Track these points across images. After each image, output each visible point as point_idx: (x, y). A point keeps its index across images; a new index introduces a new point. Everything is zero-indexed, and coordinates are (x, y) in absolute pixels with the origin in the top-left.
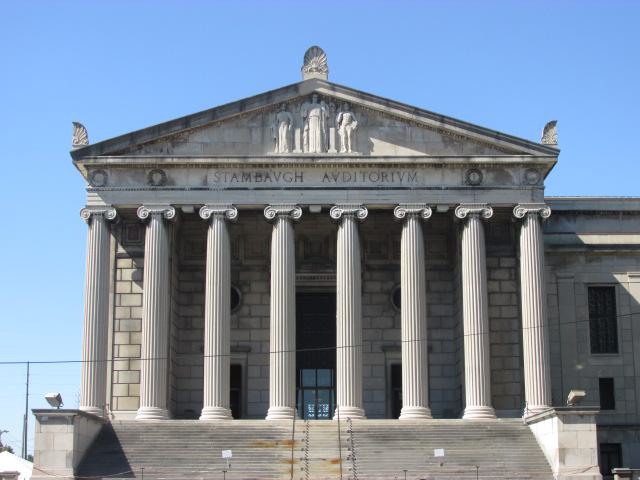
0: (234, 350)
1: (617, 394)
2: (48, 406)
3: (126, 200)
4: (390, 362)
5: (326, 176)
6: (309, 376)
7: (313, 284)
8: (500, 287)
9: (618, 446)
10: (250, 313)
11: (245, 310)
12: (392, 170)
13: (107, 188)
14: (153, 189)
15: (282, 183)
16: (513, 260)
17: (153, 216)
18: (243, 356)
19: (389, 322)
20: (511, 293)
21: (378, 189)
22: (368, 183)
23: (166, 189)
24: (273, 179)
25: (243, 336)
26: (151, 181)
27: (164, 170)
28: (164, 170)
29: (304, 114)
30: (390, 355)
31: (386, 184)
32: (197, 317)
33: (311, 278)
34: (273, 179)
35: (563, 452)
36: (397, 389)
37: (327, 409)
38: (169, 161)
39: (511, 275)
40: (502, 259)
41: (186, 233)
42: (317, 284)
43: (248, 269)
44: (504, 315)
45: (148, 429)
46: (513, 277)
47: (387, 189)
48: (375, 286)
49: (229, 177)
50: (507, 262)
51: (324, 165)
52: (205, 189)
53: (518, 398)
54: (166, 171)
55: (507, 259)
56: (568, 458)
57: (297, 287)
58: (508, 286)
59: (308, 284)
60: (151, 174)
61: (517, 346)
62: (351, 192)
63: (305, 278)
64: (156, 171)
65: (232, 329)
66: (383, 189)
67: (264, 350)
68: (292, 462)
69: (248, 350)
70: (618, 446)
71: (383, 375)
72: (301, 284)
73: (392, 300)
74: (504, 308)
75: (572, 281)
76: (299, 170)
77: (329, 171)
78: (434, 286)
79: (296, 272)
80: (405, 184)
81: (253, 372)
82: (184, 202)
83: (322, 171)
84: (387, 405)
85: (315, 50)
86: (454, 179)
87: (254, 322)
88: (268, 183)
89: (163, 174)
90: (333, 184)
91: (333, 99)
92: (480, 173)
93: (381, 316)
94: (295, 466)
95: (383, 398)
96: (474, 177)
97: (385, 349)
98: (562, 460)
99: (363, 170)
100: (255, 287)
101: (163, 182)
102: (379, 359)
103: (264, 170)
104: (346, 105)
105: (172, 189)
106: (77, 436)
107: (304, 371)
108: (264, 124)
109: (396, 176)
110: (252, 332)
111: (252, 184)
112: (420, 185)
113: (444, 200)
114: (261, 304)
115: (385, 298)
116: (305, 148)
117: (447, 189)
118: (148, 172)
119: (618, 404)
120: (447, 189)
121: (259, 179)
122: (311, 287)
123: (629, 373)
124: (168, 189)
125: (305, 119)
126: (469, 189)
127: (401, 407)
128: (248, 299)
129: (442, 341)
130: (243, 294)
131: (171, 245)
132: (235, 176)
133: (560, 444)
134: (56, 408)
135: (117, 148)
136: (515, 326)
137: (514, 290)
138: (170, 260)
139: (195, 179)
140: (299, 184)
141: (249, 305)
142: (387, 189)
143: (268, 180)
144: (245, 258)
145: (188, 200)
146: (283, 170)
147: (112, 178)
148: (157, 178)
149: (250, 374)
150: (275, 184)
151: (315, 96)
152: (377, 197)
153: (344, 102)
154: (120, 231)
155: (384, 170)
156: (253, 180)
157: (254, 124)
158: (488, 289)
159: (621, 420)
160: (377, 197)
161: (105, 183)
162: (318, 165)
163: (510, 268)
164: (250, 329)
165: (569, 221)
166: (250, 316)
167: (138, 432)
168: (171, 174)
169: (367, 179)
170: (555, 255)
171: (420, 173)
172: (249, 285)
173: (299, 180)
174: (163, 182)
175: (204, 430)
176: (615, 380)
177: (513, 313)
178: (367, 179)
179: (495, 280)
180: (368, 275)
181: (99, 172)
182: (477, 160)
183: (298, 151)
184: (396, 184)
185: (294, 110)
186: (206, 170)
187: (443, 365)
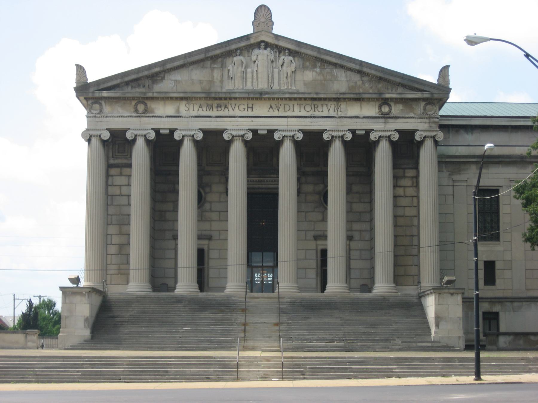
0: (200, 238)
1: (498, 273)
2: (70, 285)
3: (118, 124)
4: (320, 248)
5: (271, 107)
6: (257, 257)
7: (260, 186)
8: (404, 192)
9: (497, 314)
10: (211, 209)
11: (207, 206)
12: (322, 102)
13: (102, 115)
14: (137, 117)
15: (237, 113)
16: (415, 171)
17: (138, 137)
18: (206, 242)
19: (320, 217)
20: (413, 197)
21: (311, 117)
22: (303, 113)
23: (148, 117)
24: (230, 109)
25: (206, 226)
26: (136, 111)
27: (146, 101)
28: (146, 101)
29: (254, 58)
30: (319, 242)
31: (317, 113)
32: (169, 211)
33: (259, 181)
34: (230, 109)
35: (438, 319)
36: (324, 268)
37: (271, 276)
38: (150, 95)
39: (413, 183)
40: (407, 171)
41: (164, 148)
42: (264, 186)
43: (209, 173)
44: (407, 214)
45: (139, 299)
46: (415, 185)
47: (318, 117)
48: (309, 188)
49: (196, 107)
50: (410, 173)
51: (269, 99)
52: (178, 117)
53: (416, 277)
54: (149, 103)
55: (411, 171)
56: (442, 325)
57: (248, 188)
58: (410, 191)
59: (257, 186)
60: (136, 105)
61: (416, 238)
62: (290, 119)
63: (253, 181)
64: (140, 102)
65: (198, 221)
66: (315, 117)
67: (222, 237)
68: (245, 324)
69: (210, 238)
70: (497, 314)
71: (315, 258)
72: (251, 186)
73: (322, 199)
74: (407, 209)
75: (465, 184)
76: (250, 102)
77: (273, 103)
78: (355, 188)
79: (248, 177)
80: (332, 113)
81: (213, 254)
82: (162, 127)
83: (267, 104)
84: (317, 281)
85: (263, 8)
86: (371, 110)
87: (214, 216)
88: (226, 113)
89: (146, 105)
90: (276, 113)
91: (277, 46)
92: (390, 106)
93: (314, 211)
94: (247, 328)
95: (314, 276)
96: (385, 109)
97: (316, 238)
98: (437, 325)
99: (300, 102)
100: (215, 188)
101: (146, 111)
102: (312, 245)
103: (223, 102)
104: (287, 51)
105: (153, 117)
106: (91, 305)
107: (253, 253)
108: (223, 66)
109: (325, 108)
110: (213, 223)
111: (215, 113)
112: (343, 115)
113: (361, 126)
114: (220, 220)
115: (317, 197)
116: (255, 84)
117: (364, 117)
118: (134, 103)
119: (497, 281)
120: (364, 117)
121: (219, 109)
122: (259, 188)
123: (508, 257)
124: (150, 117)
125: (254, 62)
126: (382, 118)
127: (327, 284)
128: (210, 197)
129: (360, 231)
130: (206, 193)
131: (151, 158)
132: (201, 106)
133: (435, 314)
134: (75, 286)
135: (110, 84)
136: (415, 222)
137: (415, 194)
138: (151, 169)
139: (169, 109)
140: (250, 113)
141: (210, 202)
142: (318, 117)
143: (226, 110)
144: (207, 165)
145: (165, 125)
146: (238, 102)
147: (107, 109)
148: (141, 108)
149: (211, 256)
150: (231, 113)
151: (263, 44)
152: (310, 124)
153: (285, 49)
154: (111, 146)
155: (315, 102)
156: (215, 109)
157: (215, 66)
158: (394, 193)
159: (500, 294)
160: (310, 124)
161: (101, 111)
162: (265, 99)
163: (412, 177)
164: (211, 221)
165: (468, 134)
166: (211, 211)
167: (129, 301)
168: (152, 105)
169: (302, 109)
170: (448, 164)
171: (343, 105)
172: (210, 186)
173: (250, 110)
174: (146, 111)
175: (179, 300)
176: (497, 263)
177: (413, 212)
178: (302, 109)
179: (400, 187)
180: (303, 179)
181: (96, 103)
182: (387, 96)
183: (249, 86)
184: (325, 113)
185: (246, 55)
186: (178, 101)
187: (360, 250)
